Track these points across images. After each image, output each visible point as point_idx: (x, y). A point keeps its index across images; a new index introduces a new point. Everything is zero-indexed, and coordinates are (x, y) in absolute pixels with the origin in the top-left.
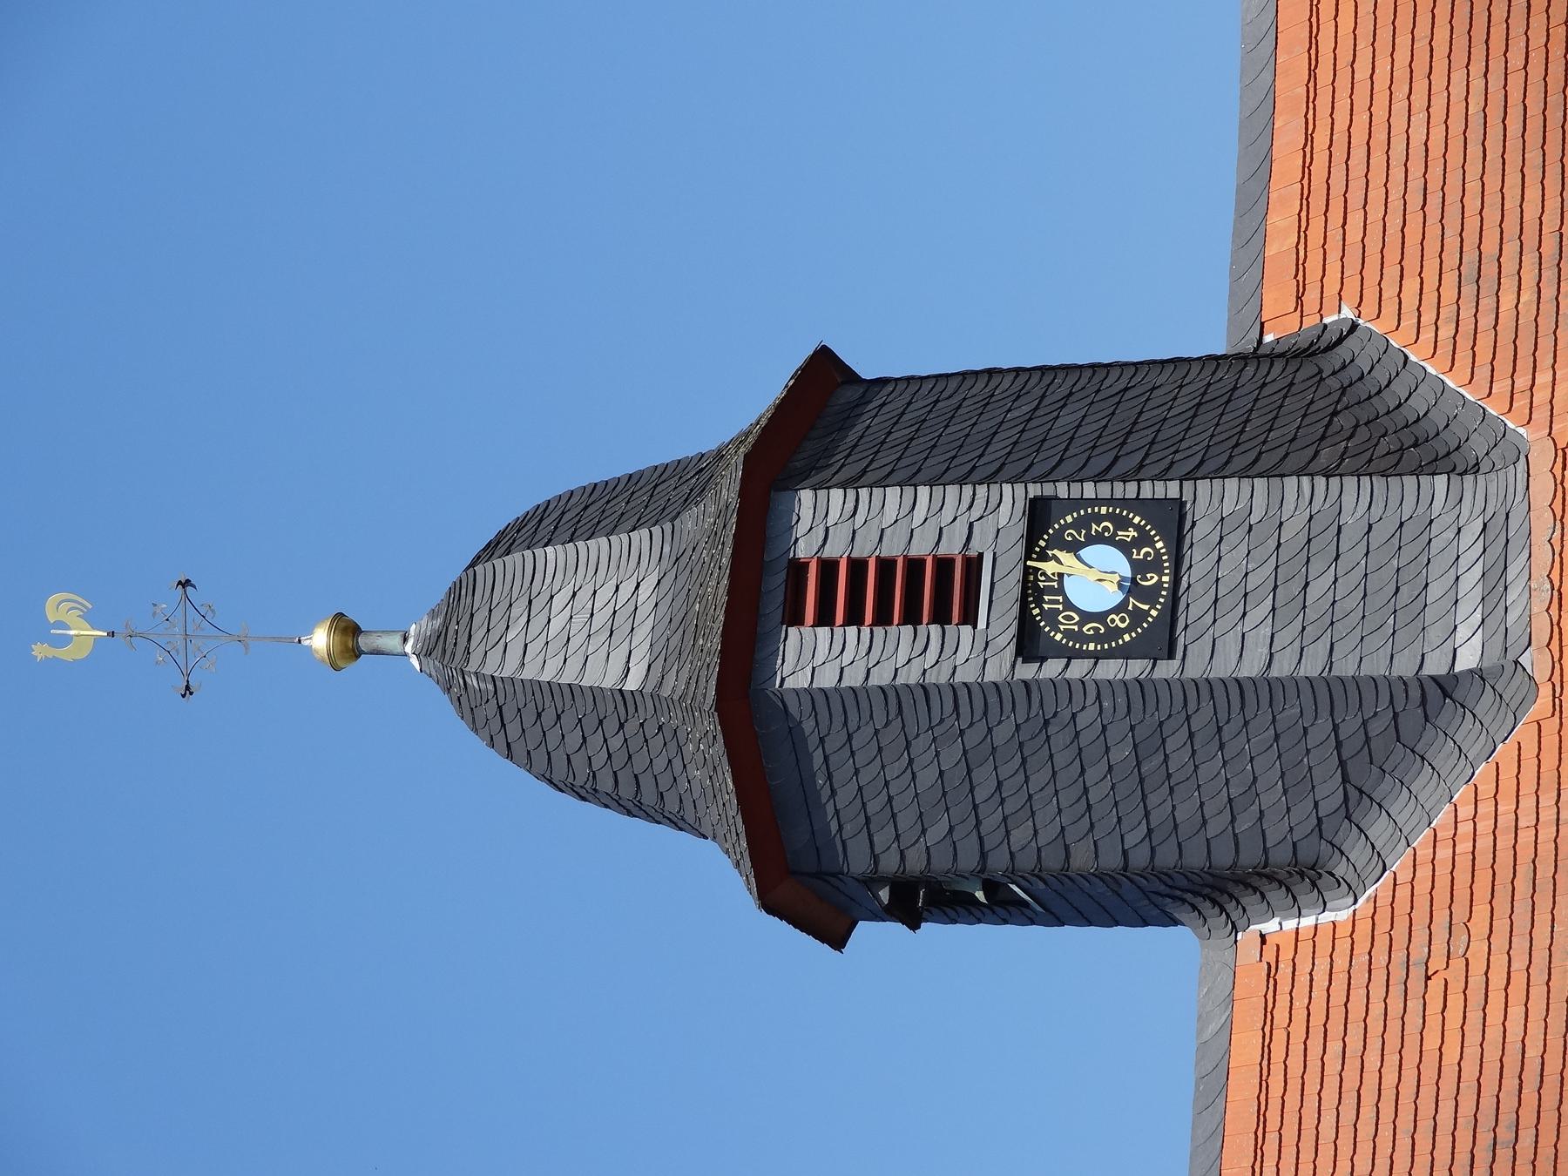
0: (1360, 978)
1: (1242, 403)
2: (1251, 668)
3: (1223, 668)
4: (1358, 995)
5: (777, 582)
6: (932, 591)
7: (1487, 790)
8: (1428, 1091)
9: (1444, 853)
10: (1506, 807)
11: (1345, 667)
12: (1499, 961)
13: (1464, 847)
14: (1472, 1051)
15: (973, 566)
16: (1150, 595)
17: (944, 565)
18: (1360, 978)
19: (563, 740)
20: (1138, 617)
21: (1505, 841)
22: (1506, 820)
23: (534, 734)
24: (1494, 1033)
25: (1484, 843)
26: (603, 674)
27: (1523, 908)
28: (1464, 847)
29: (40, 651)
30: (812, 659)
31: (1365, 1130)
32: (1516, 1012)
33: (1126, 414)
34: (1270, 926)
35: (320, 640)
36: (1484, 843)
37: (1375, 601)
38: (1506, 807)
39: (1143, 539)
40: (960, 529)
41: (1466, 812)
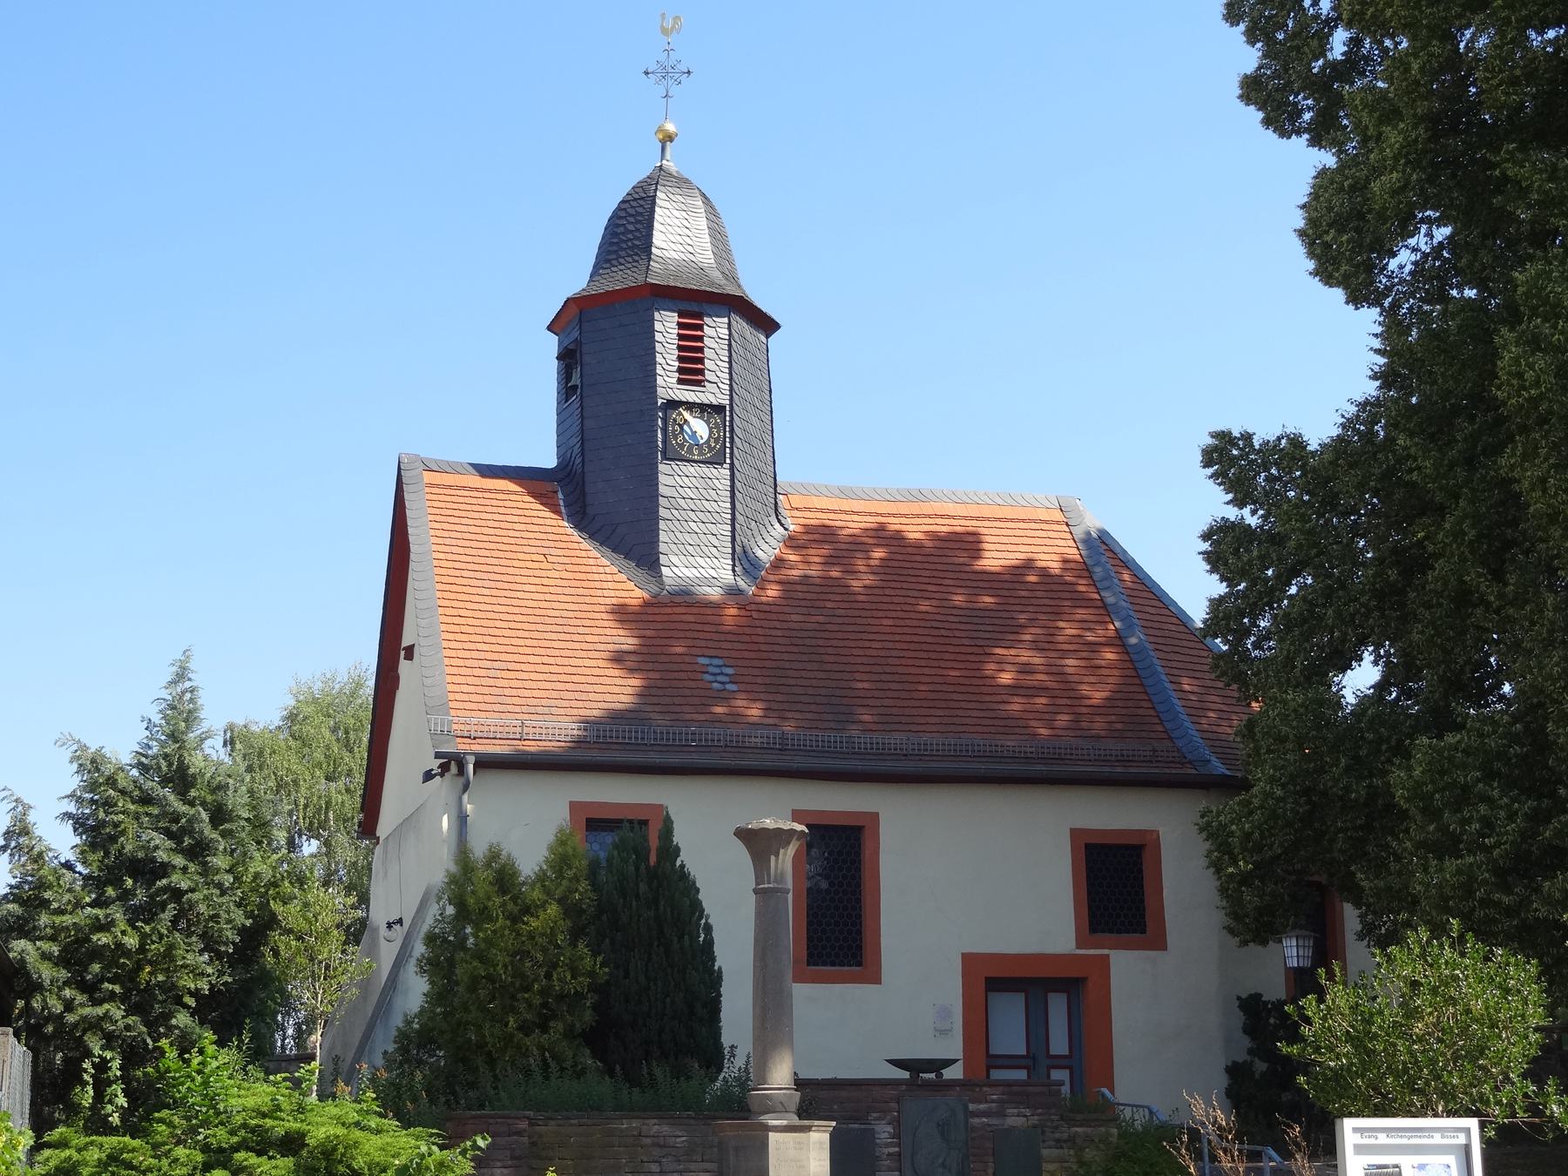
0: (542, 529)
1: (760, 486)
2: (662, 490)
3: (662, 478)
4: (536, 528)
5: (694, 307)
6: (691, 371)
7: (616, 578)
8: (501, 554)
9: (592, 562)
10: (610, 585)
11: (662, 525)
13: (594, 569)
14: (517, 571)
15: (699, 383)
16: (690, 450)
17: (701, 372)
18: (542, 529)
19: (630, 228)
21: (597, 585)
22: (605, 585)
23: (632, 211)
24: (525, 580)
25: (596, 577)
26: (658, 239)
27: (572, 591)
28: (594, 569)
29: (1105, 1090)
30: (666, 326)
31: (486, 530)
32: (533, 588)
33: (756, 442)
34: (560, 496)
35: (670, 127)
36: (596, 577)
37: (687, 536)
38: (610, 585)
39: (711, 449)
40: (714, 379)
41: (608, 570)
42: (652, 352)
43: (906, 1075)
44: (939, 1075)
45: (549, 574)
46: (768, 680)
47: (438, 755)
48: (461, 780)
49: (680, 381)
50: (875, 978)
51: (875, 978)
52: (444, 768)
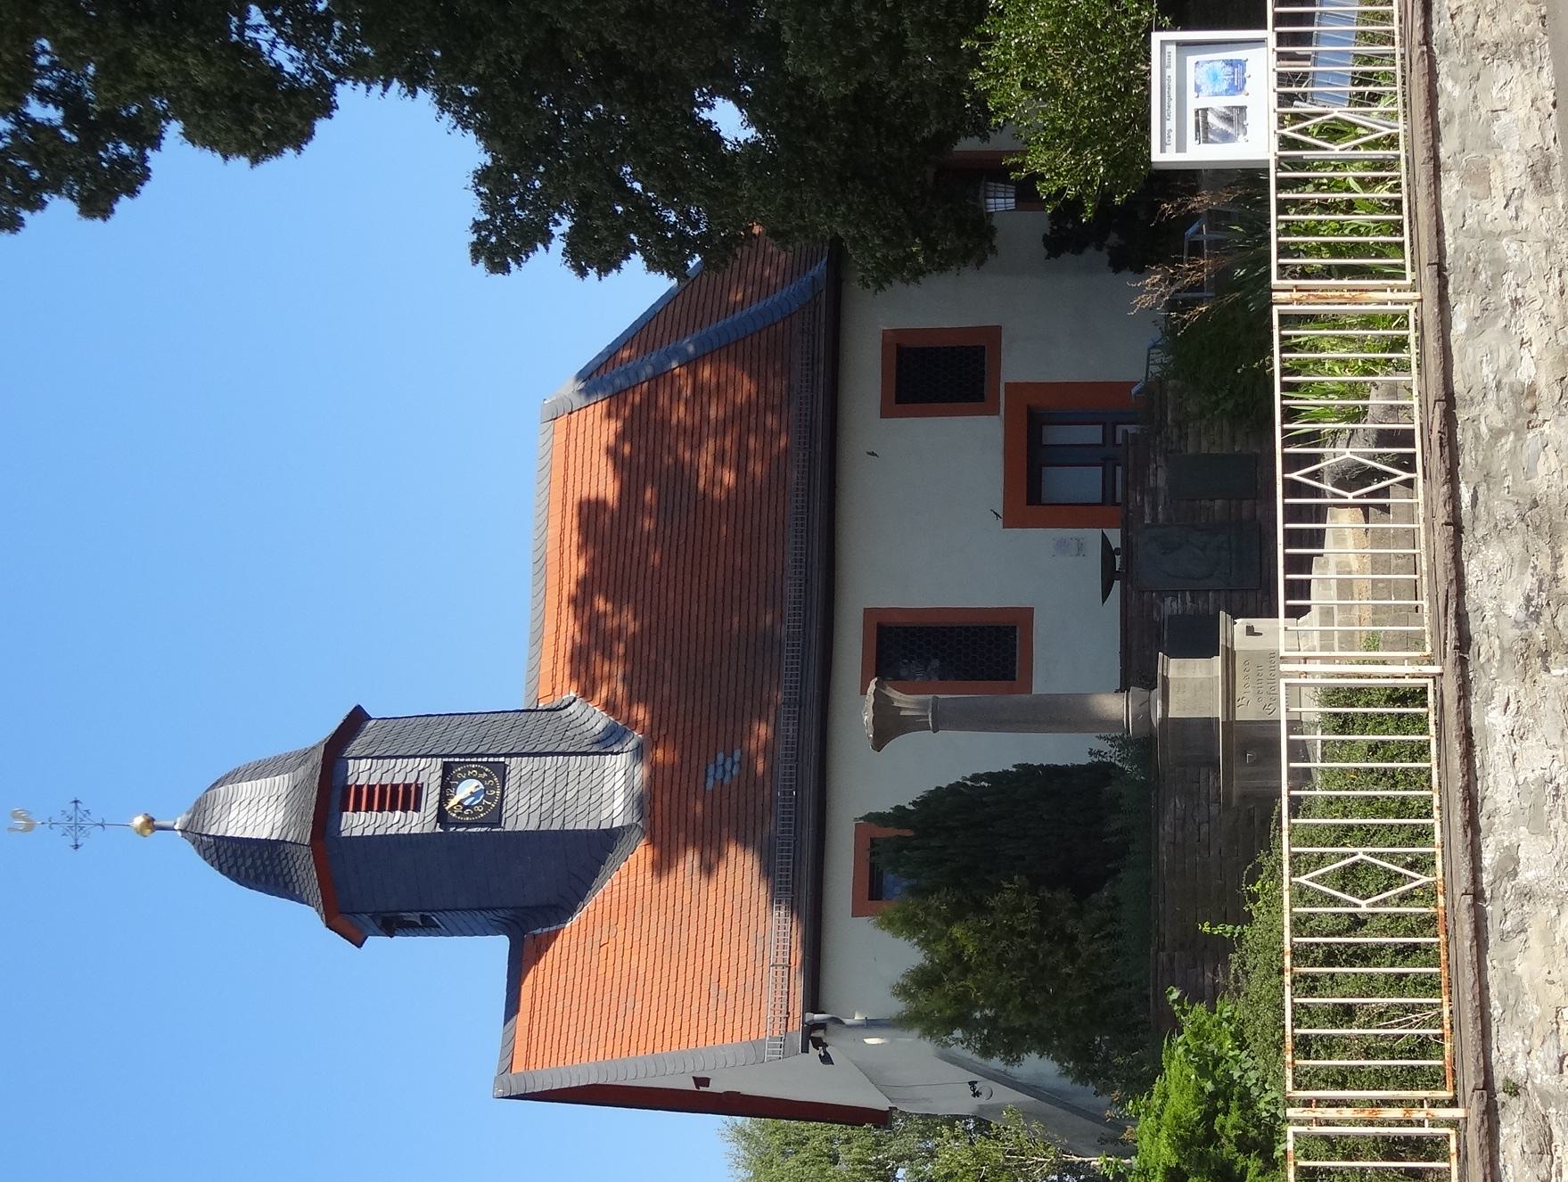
2: (532, 827)
6: (406, 797)
7: (624, 873)
12: (629, 938)
15: (419, 790)
16: (491, 799)
17: (407, 787)
20: (487, 807)
30: (357, 823)
35: (139, 821)
39: (489, 777)
42: (385, 838)
43: (1117, 584)
44: (1117, 551)
45: (620, 941)
46: (730, 719)
47: (805, 1050)
48: (831, 1026)
49: (417, 809)
50: (1027, 614)
51: (1027, 614)
52: (818, 1043)
